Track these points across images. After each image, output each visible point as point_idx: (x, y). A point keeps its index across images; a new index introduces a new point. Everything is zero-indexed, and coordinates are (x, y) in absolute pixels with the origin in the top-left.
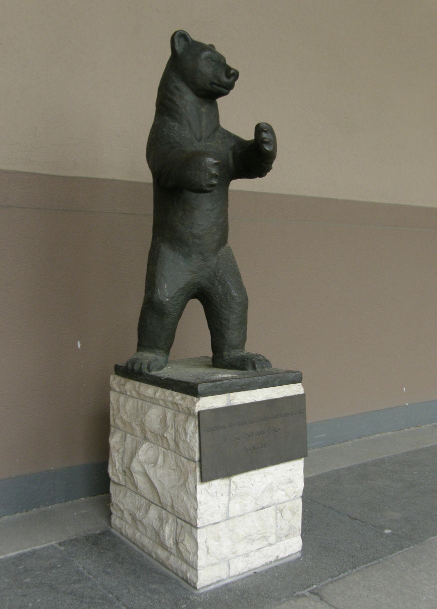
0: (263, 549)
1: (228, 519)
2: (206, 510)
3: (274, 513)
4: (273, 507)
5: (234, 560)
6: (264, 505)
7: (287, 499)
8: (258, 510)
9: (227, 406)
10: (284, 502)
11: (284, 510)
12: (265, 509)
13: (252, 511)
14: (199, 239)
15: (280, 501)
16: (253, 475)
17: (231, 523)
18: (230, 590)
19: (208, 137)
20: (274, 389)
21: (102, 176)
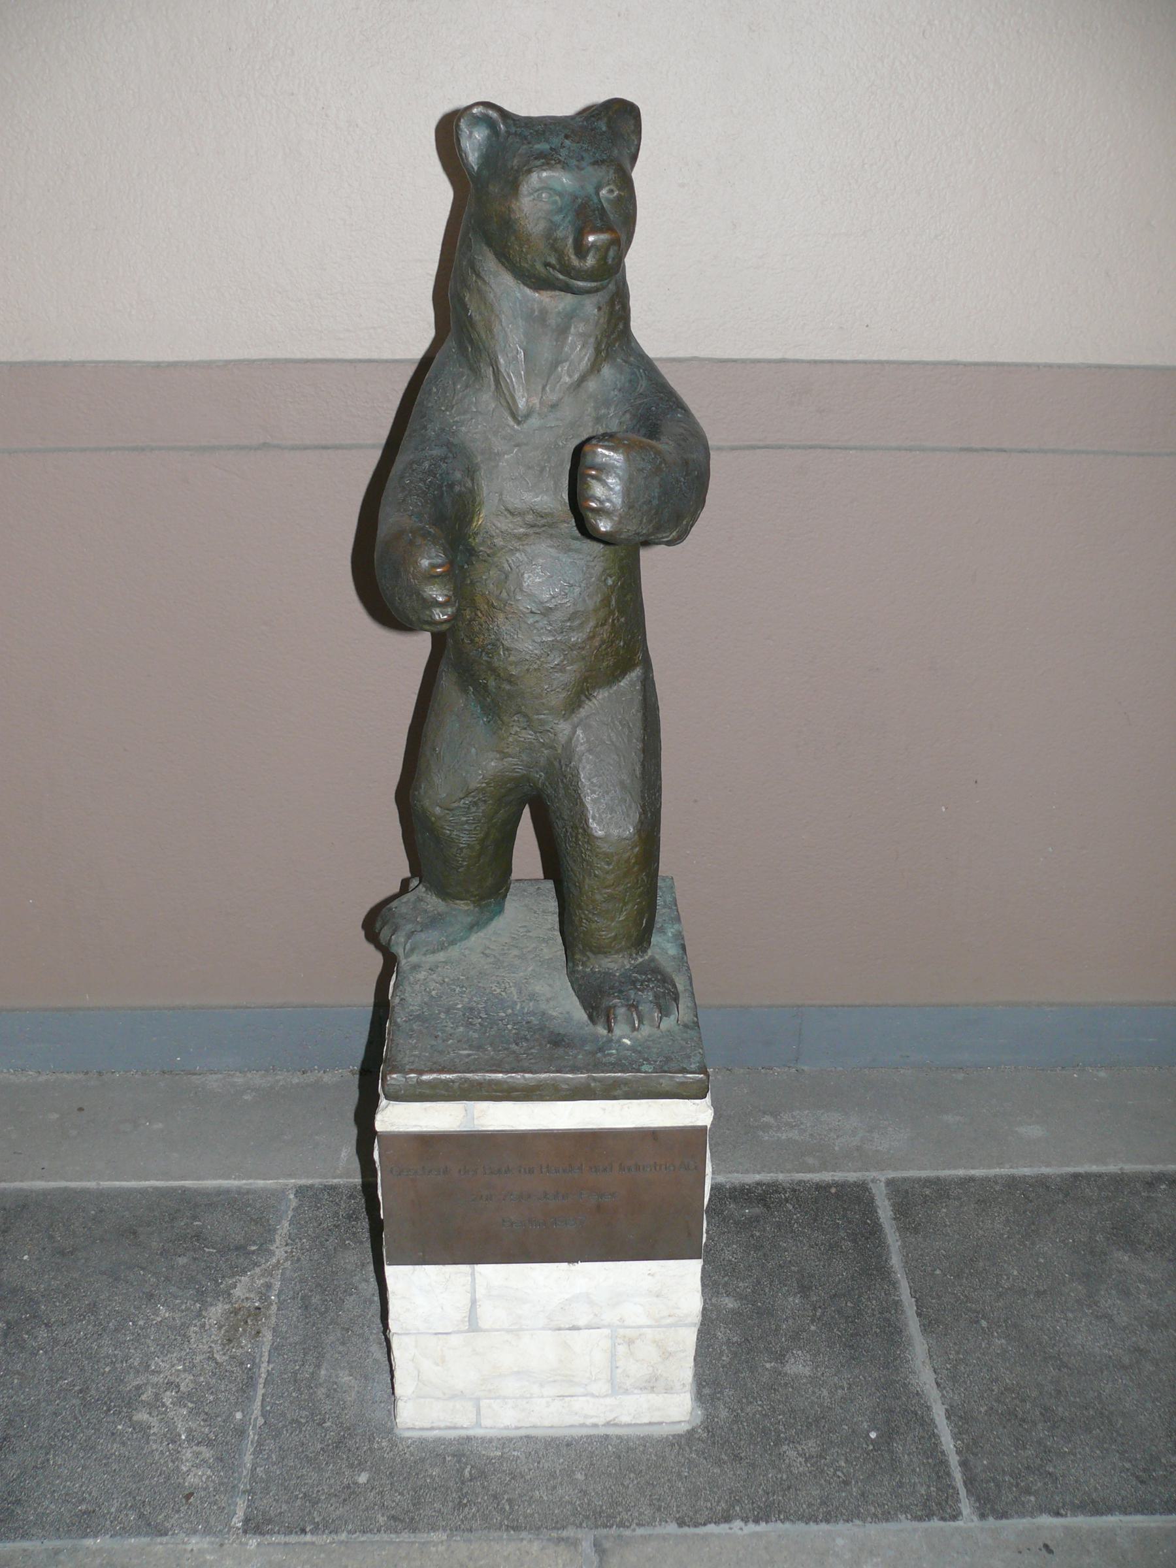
4: (607, 1331)
8: (560, 1329)
10: (640, 1327)
13: (543, 1329)
14: (510, 682)
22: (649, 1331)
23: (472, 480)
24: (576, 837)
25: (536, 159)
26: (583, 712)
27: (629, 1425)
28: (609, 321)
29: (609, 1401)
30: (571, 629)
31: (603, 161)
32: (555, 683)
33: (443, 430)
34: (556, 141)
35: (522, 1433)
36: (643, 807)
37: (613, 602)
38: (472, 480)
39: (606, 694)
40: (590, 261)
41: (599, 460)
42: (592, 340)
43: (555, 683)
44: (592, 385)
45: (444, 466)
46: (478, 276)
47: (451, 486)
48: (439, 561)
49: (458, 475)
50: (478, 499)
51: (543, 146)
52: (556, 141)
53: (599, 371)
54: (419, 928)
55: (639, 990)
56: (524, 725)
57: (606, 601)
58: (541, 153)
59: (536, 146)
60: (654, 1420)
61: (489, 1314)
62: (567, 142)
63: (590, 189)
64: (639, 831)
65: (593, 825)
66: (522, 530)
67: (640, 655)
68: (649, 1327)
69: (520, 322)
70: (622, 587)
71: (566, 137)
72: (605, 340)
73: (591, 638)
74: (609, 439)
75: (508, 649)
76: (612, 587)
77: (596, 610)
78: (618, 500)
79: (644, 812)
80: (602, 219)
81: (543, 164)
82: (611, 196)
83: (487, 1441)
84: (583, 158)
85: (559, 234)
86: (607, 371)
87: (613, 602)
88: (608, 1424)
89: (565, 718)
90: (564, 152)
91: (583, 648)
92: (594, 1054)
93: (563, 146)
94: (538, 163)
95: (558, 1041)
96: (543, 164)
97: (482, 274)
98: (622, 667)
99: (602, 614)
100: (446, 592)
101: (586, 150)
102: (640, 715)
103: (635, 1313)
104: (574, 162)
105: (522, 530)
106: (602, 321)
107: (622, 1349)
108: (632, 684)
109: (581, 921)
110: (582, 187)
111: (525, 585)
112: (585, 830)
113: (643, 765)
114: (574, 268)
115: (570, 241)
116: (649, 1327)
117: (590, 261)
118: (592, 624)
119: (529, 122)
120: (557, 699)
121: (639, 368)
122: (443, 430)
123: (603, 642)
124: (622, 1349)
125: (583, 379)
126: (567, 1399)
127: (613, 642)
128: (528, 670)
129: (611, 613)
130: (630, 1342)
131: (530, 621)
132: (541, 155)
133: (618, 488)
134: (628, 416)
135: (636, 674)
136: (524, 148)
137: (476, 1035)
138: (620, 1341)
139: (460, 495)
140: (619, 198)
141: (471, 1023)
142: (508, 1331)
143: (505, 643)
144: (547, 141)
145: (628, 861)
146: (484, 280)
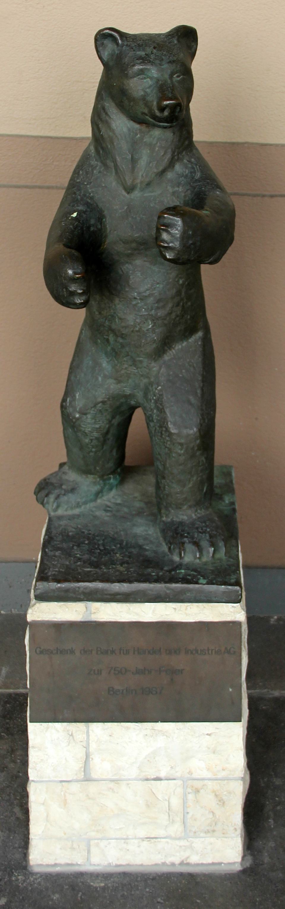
0: (156, 840)
1: (88, 779)
2: (42, 760)
3: (180, 790)
4: (179, 782)
5: (99, 841)
6: (162, 775)
7: (209, 775)
8: (147, 780)
9: (83, 620)
10: (203, 779)
11: (202, 791)
12: (162, 781)
13: (136, 779)
14: (122, 338)
15: (195, 776)
16: (128, 728)
17: (92, 788)
18: (73, 887)
19: (148, 184)
20: (181, 605)
21: (250, 140)
22: (210, 783)
23: (101, 224)
24: (161, 433)
25: (137, 59)
26: (166, 357)
27: (198, 865)
28: (179, 140)
29: (182, 843)
30: (158, 308)
31: (174, 61)
32: (149, 339)
33: (85, 195)
34: (149, 50)
35: (121, 869)
36: (202, 415)
37: (183, 294)
38: (101, 224)
39: (180, 347)
40: (166, 113)
41: (166, 221)
42: (170, 150)
43: (149, 339)
44: (170, 175)
45: (84, 216)
46: (107, 114)
47: (89, 228)
48: (79, 271)
49: (92, 222)
50: (104, 234)
51: (142, 53)
52: (149, 50)
53: (174, 166)
54: (63, 492)
55: (200, 533)
56: (130, 363)
57: (179, 293)
58: (141, 56)
59: (138, 53)
60: (216, 861)
61: (101, 767)
62: (155, 51)
63: (167, 76)
64: (200, 430)
65: (170, 426)
66: (129, 251)
67: (201, 324)
68: (209, 779)
69: (87, 327)
70: (188, 284)
71: (155, 48)
72: (177, 150)
73: (170, 314)
74: (174, 210)
75: (120, 319)
76: (182, 285)
77: (173, 298)
78: (177, 244)
79: (203, 419)
80: (172, 93)
81: (141, 63)
82: (179, 79)
83: (95, 876)
84: (163, 60)
85: (149, 98)
86: (178, 167)
87: (183, 294)
88: (182, 863)
89: (155, 360)
90: (152, 57)
91: (165, 319)
92: (170, 571)
93: (152, 53)
94: (139, 62)
95: (147, 562)
96: (141, 63)
97: (109, 113)
98: (190, 331)
99: (176, 300)
100: (82, 288)
101: (165, 55)
102: (200, 359)
103: (199, 767)
104: (157, 62)
105: (129, 251)
106: (175, 140)
107: (191, 797)
108: (196, 341)
109: (164, 488)
110: (162, 75)
111: (131, 282)
112: (166, 429)
113: (202, 390)
114: (157, 117)
115: (155, 103)
116: (209, 779)
117: (166, 113)
118: (170, 305)
119: (135, 37)
120: (150, 348)
121: (196, 165)
122: (85, 195)
123: (177, 316)
124: (191, 797)
125: (164, 171)
126: (153, 840)
127: (183, 316)
128: (132, 331)
129: (182, 299)
130: (197, 791)
131: (134, 303)
132: (140, 58)
133: (178, 236)
134: (189, 192)
135: (200, 334)
136: (131, 54)
137: (95, 560)
138: (189, 790)
139: (94, 232)
140: (183, 79)
141: (93, 553)
142: (112, 781)
143: (119, 315)
144: (144, 50)
145: (193, 448)
146: (110, 117)
